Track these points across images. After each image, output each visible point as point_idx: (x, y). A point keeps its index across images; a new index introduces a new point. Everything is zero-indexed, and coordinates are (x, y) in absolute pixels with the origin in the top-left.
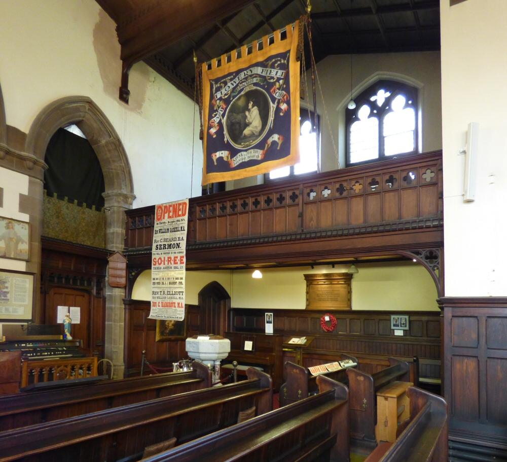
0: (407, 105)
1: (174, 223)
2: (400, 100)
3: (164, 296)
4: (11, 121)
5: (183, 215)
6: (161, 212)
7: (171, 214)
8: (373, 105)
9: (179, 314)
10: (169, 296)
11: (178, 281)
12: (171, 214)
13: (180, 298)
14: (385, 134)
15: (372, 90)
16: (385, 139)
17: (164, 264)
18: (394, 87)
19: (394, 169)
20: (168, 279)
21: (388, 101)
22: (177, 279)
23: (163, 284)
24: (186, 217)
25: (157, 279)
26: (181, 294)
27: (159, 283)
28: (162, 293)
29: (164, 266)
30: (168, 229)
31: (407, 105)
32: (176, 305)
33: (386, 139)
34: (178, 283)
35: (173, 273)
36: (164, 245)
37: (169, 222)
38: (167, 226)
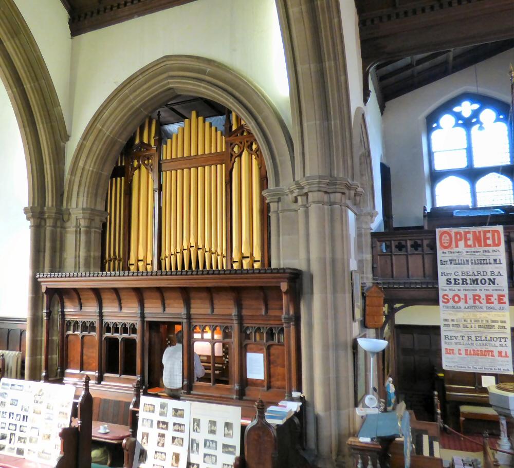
0: (498, 120)
1: (477, 254)
2: (488, 115)
3: (470, 341)
4: (503, 128)
5: (499, 245)
6: (448, 238)
7: (470, 242)
8: (458, 116)
9: (502, 365)
10: (480, 342)
11: (496, 325)
12: (470, 242)
13: (501, 345)
14: (434, 150)
15: (457, 100)
16: (435, 154)
17: (466, 302)
18: (485, 101)
19: (84, 177)
20: (476, 321)
21: (476, 114)
22: (493, 321)
23: (465, 326)
24: (502, 248)
25: (453, 320)
26: (503, 340)
27: (458, 326)
28: (466, 338)
29: (466, 305)
30: (467, 261)
31: (498, 120)
32: (496, 354)
33: (435, 155)
34: (451, 326)
35: (484, 315)
36: (462, 279)
37: (467, 252)
38: (464, 256)
